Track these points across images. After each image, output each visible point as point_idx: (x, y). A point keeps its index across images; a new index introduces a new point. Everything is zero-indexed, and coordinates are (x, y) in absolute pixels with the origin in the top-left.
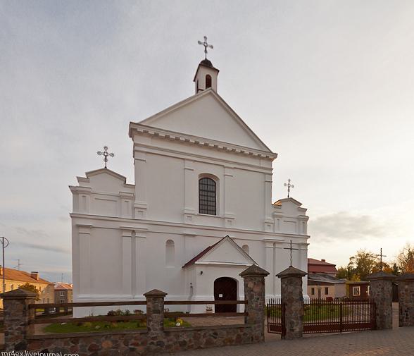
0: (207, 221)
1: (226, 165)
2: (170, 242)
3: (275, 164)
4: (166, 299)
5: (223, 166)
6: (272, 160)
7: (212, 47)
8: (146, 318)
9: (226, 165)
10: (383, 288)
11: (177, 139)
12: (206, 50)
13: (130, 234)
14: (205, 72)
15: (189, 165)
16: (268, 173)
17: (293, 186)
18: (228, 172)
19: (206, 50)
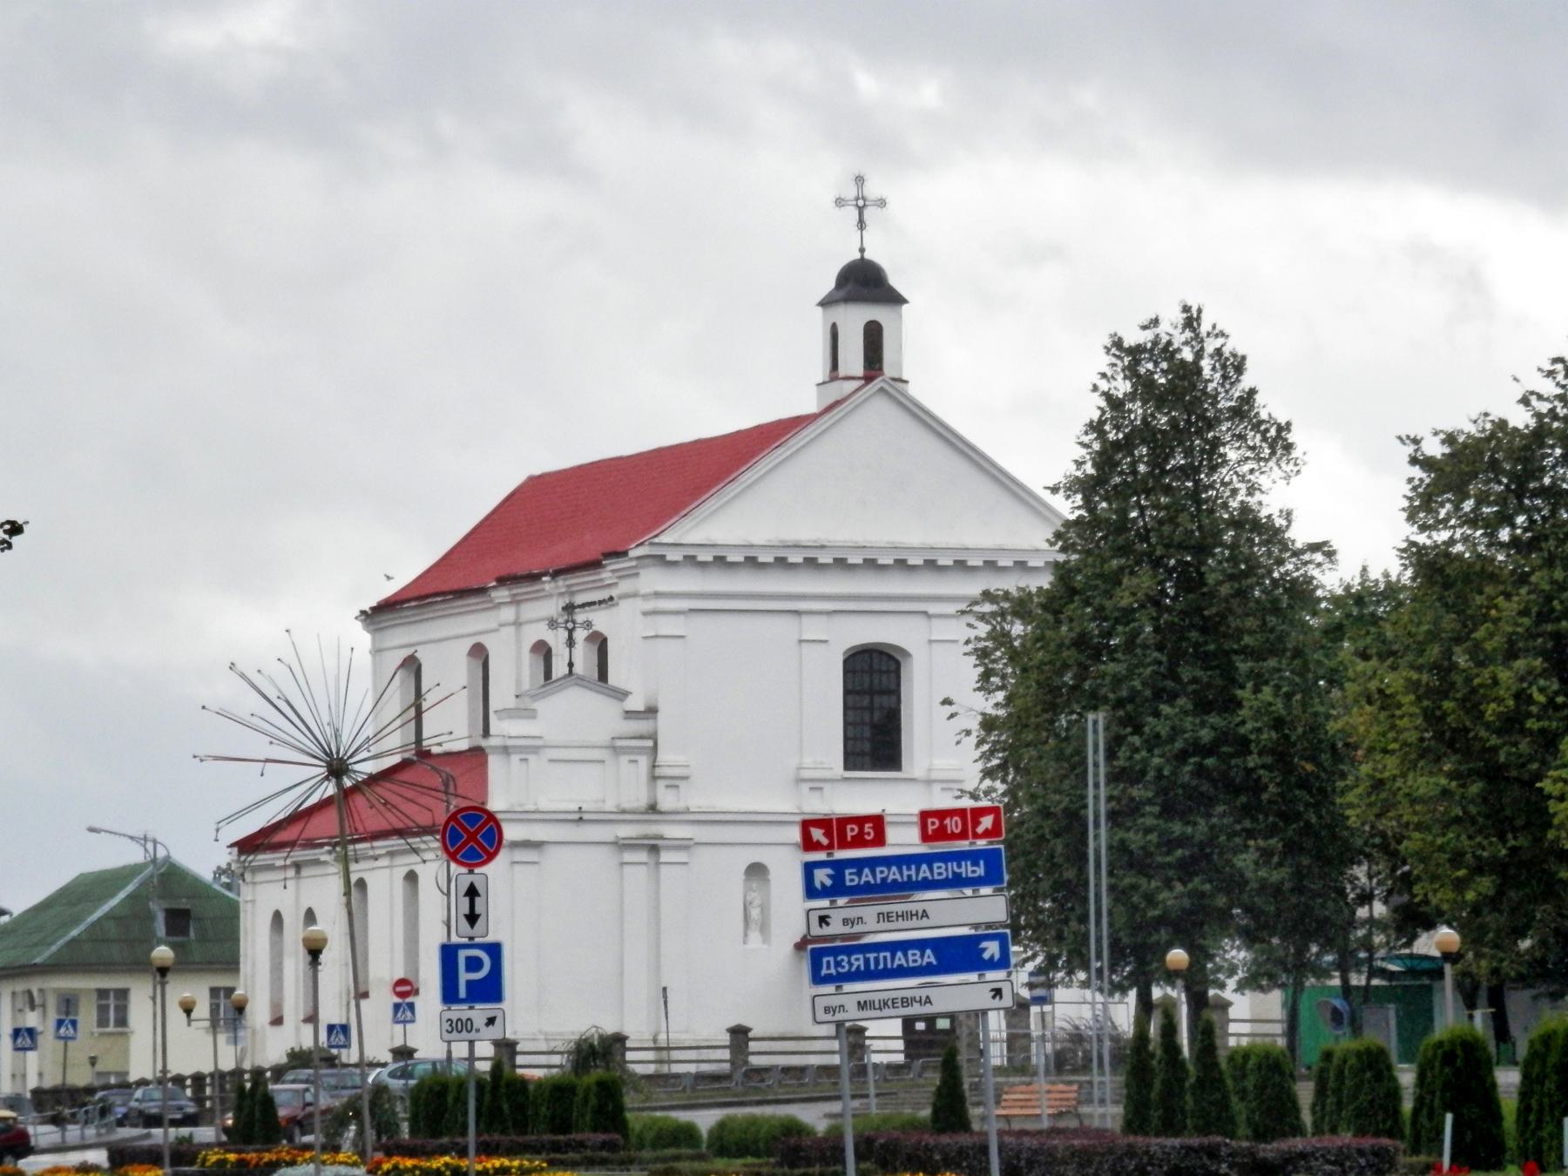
1: (933, 608)
5: (925, 613)
9: (933, 608)
13: (642, 856)
14: (853, 319)
15: (814, 628)
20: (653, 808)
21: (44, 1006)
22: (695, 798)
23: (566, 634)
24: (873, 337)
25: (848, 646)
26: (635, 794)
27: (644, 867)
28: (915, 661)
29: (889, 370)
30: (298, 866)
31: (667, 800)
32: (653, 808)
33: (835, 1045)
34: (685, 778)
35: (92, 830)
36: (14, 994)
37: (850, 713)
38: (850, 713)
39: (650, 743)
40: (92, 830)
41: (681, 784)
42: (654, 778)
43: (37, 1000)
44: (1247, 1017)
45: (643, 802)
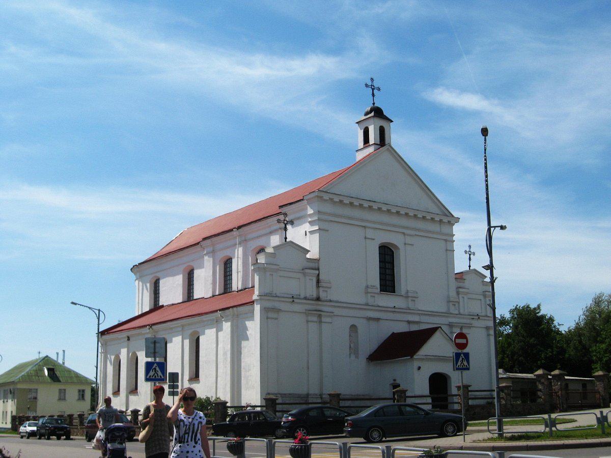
0: (387, 300)
2: (353, 328)
3: (456, 229)
4: (470, 389)
6: (451, 224)
7: (379, 89)
8: (584, 347)
10: (253, 354)
11: (389, 211)
12: (470, 258)
15: (370, 233)
16: (449, 239)
17: (474, 254)
18: (409, 240)
19: (470, 258)
20: (318, 299)
21: (14, 393)
22: (333, 295)
23: (469, 256)
24: (382, 132)
25: (385, 128)
26: (312, 291)
27: (315, 323)
28: (401, 250)
29: (387, 142)
30: (183, 326)
31: (323, 295)
32: (318, 299)
33: (504, 431)
34: (330, 288)
35: (73, 303)
36: (4, 390)
37: (381, 264)
38: (381, 264)
39: (317, 272)
40: (73, 303)
41: (329, 290)
42: (318, 286)
43: (12, 392)
44: (259, 405)
45: (315, 296)
